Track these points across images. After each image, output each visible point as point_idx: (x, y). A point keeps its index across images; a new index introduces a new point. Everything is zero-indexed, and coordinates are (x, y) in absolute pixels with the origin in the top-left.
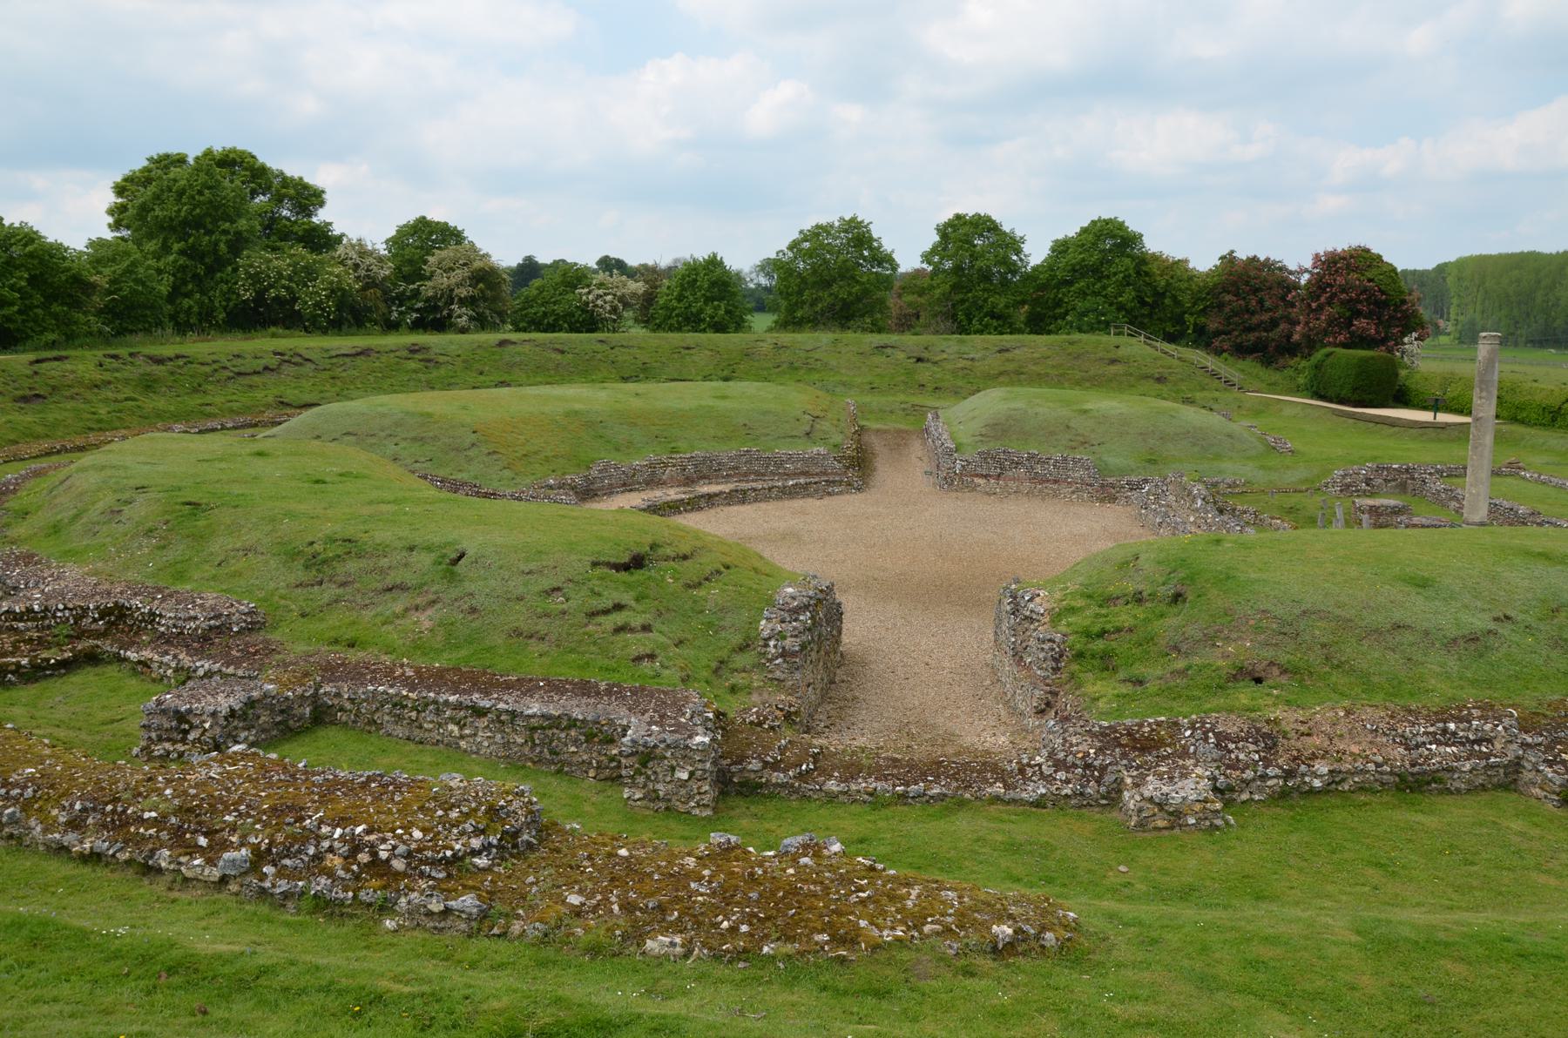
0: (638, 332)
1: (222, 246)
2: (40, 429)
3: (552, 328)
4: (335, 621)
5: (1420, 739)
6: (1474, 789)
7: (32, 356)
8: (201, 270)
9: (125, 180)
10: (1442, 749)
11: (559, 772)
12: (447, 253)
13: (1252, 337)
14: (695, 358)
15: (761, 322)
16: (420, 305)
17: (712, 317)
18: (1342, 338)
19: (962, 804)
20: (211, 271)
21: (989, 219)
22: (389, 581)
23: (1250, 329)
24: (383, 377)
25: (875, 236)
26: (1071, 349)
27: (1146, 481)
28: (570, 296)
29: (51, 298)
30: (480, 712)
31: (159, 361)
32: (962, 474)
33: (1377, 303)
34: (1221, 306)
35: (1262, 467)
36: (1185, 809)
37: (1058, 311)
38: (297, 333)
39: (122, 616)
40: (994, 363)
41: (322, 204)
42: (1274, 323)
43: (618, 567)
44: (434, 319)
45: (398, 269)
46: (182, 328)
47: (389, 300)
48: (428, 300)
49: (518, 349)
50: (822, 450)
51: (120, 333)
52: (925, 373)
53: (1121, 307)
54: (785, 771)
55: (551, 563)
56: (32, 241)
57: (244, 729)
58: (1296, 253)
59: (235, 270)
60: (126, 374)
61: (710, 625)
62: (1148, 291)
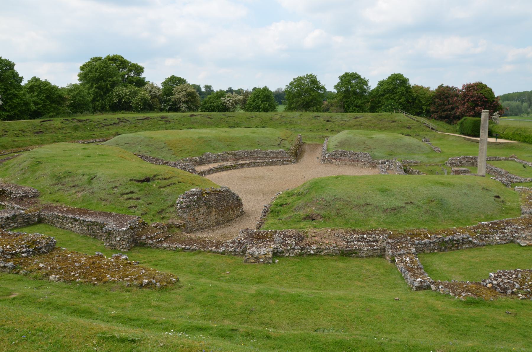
0: (242, 111)
1: (109, 86)
2: (39, 142)
3: (212, 111)
4: (57, 196)
5: (352, 240)
6: (368, 257)
7: (42, 120)
8: (102, 93)
9: (84, 66)
10: (359, 243)
11: (95, 238)
12: (180, 86)
13: (445, 113)
14: (254, 120)
16: (171, 103)
17: (263, 107)
18: (471, 113)
19: (200, 252)
20: (105, 93)
21: (357, 74)
22: (74, 184)
23: (444, 111)
24: (152, 126)
25: (318, 80)
26: (379, 117)
27: (387, 161)
28: (218, 101)
29: (53, 102)
30: (76, 220)
31: (81, 121)
32: (326, 160)
33: (484, 102)
34: (435, 103)
35: (428, 157)
36: (259, 256)
37: (379, 105)
38: (130, 112)
39: (4, 193)
40: (353, 122)
41: (143, 72)
42: (453, 109)
43: (139, 181)
44: (175, 108)
45: (165, 92)
46: (95, 110)
47: (161, 102)
48: (173, 102)
49: (197, 117)
50: (282, 150)
51: (75, 113)
52: (329, 126)
53: (400, 103)
54: (153, 240)
55: (118, 179)
56: (47, 85)
57: (13, 223)
58: (458, 82)
59: (112, 93)
60: (69, 125)
61: (163, 199)
62: (410, 98)
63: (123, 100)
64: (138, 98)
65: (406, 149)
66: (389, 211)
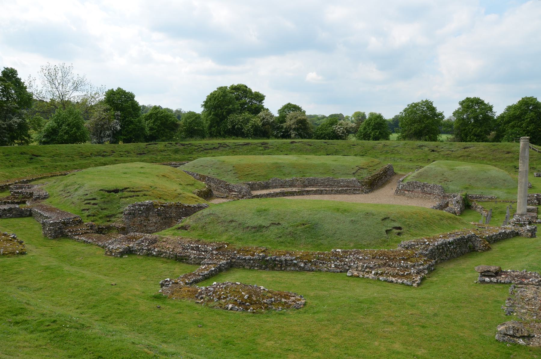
1: (224, 113)
3: (324, 138)
8: (218, 120)
15: (394, 136)
20: (222, 120)
21: (479, 99)
31: (183, 145)
32: (400, 192)
40: (460, 152)
44: (286, 135)
49: (297, 144)
60: (171, 148)
63: (236, 127)
64: (249, 125)
65: (488, 183)
66: (250, 228)
